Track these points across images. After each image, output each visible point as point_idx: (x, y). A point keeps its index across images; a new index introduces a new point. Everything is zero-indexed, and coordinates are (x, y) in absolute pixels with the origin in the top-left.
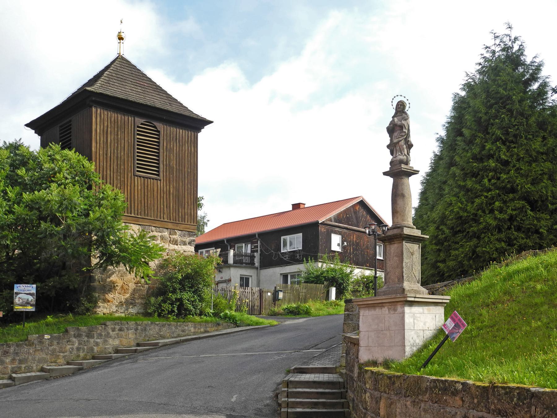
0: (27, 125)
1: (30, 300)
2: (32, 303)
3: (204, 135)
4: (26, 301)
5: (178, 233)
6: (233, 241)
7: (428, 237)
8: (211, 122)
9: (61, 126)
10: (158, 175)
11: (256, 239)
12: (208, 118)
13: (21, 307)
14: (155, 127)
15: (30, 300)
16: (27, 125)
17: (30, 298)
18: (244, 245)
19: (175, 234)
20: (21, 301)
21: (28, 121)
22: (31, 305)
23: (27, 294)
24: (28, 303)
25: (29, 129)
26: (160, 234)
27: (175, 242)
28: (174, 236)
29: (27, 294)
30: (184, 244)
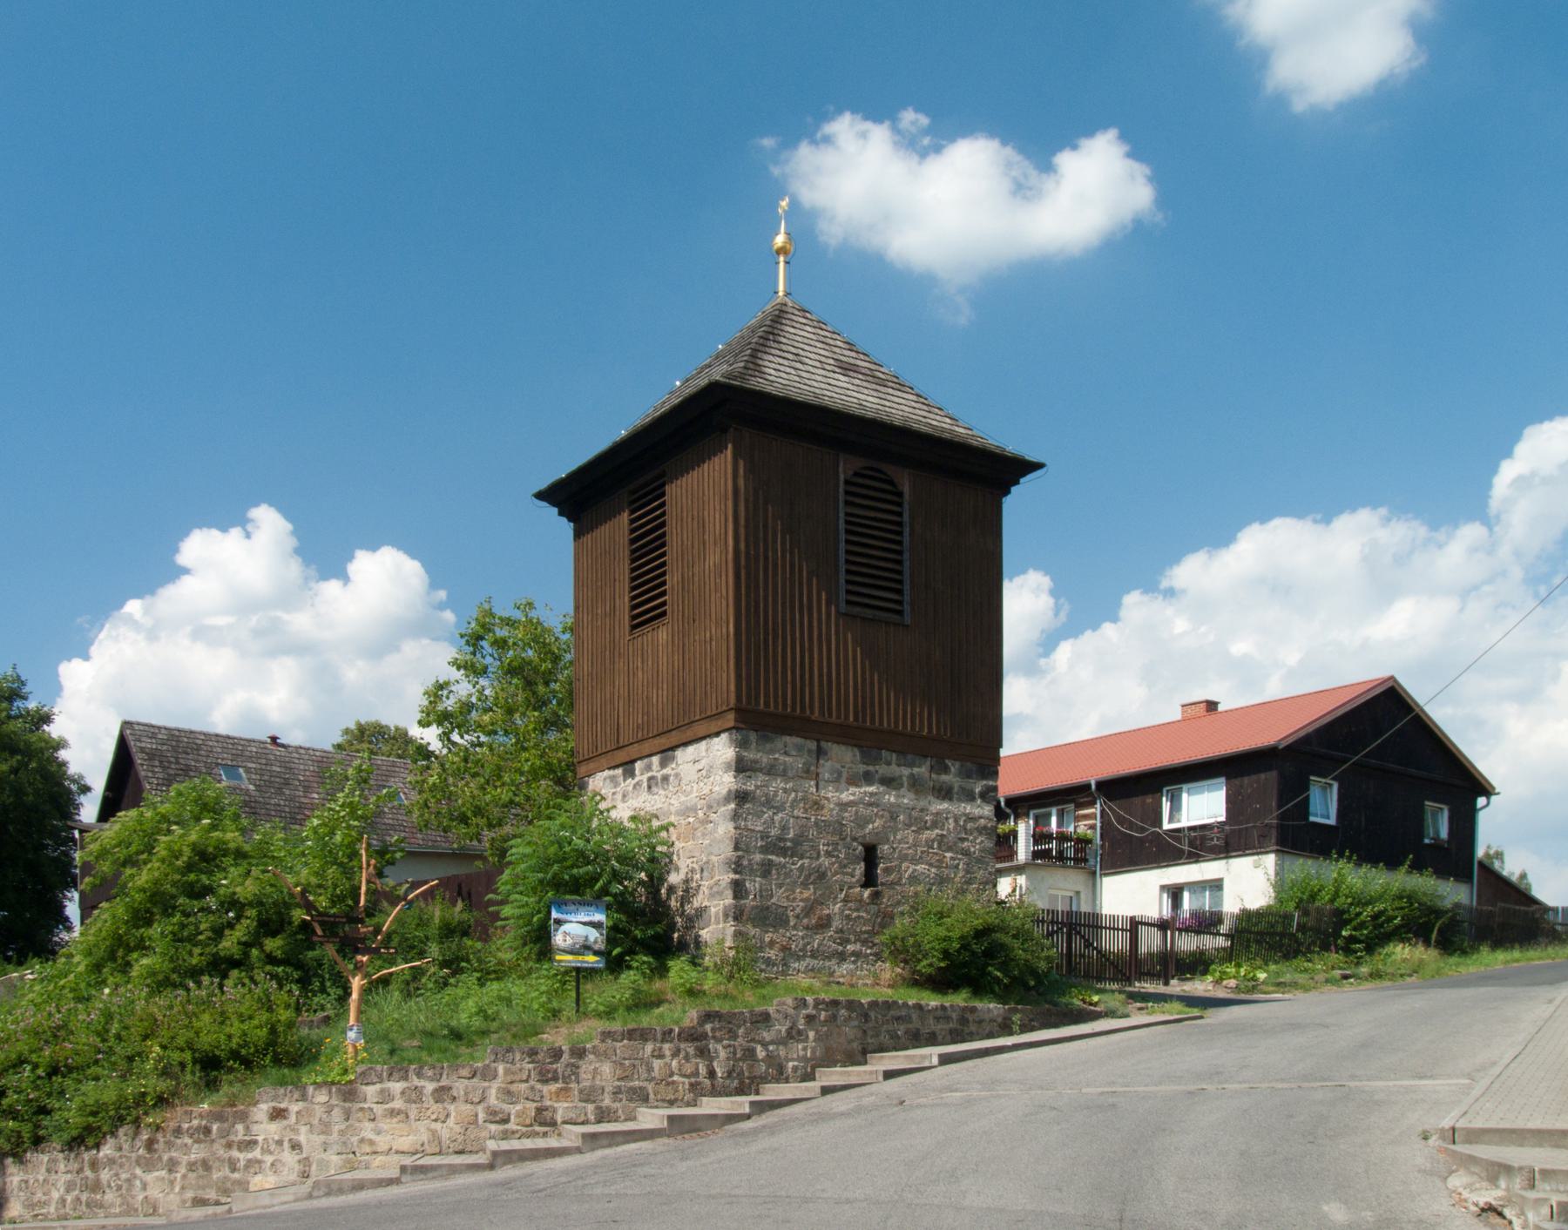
0: (540, 496)
1: (592, 939)
2: (596, 947)
3: (1018, 505)
4: (581, 940)
5: (954, 766)
6: (1072, 796)
7: (1444, 834)
8: (1038, 466)
9: (633, 492)
10: (900, 613)
11: (1091, 794)
12: (1031, 455)
13: (570, 957)
14: (891, 482)
15: (592, 939)
16: (540, 496)
17: (593, 934)
18: (1054, 811)
19: (946, 770)
20: (569, 941)
21: (544, 483)
22: (596, 953)
23: (585, 924)
24: (586, 948)
25: (545, 504)
26: (906, 771)
27: (945, 793)
28: (944, 778)
29: (585, 924)
30: (970, 797)
